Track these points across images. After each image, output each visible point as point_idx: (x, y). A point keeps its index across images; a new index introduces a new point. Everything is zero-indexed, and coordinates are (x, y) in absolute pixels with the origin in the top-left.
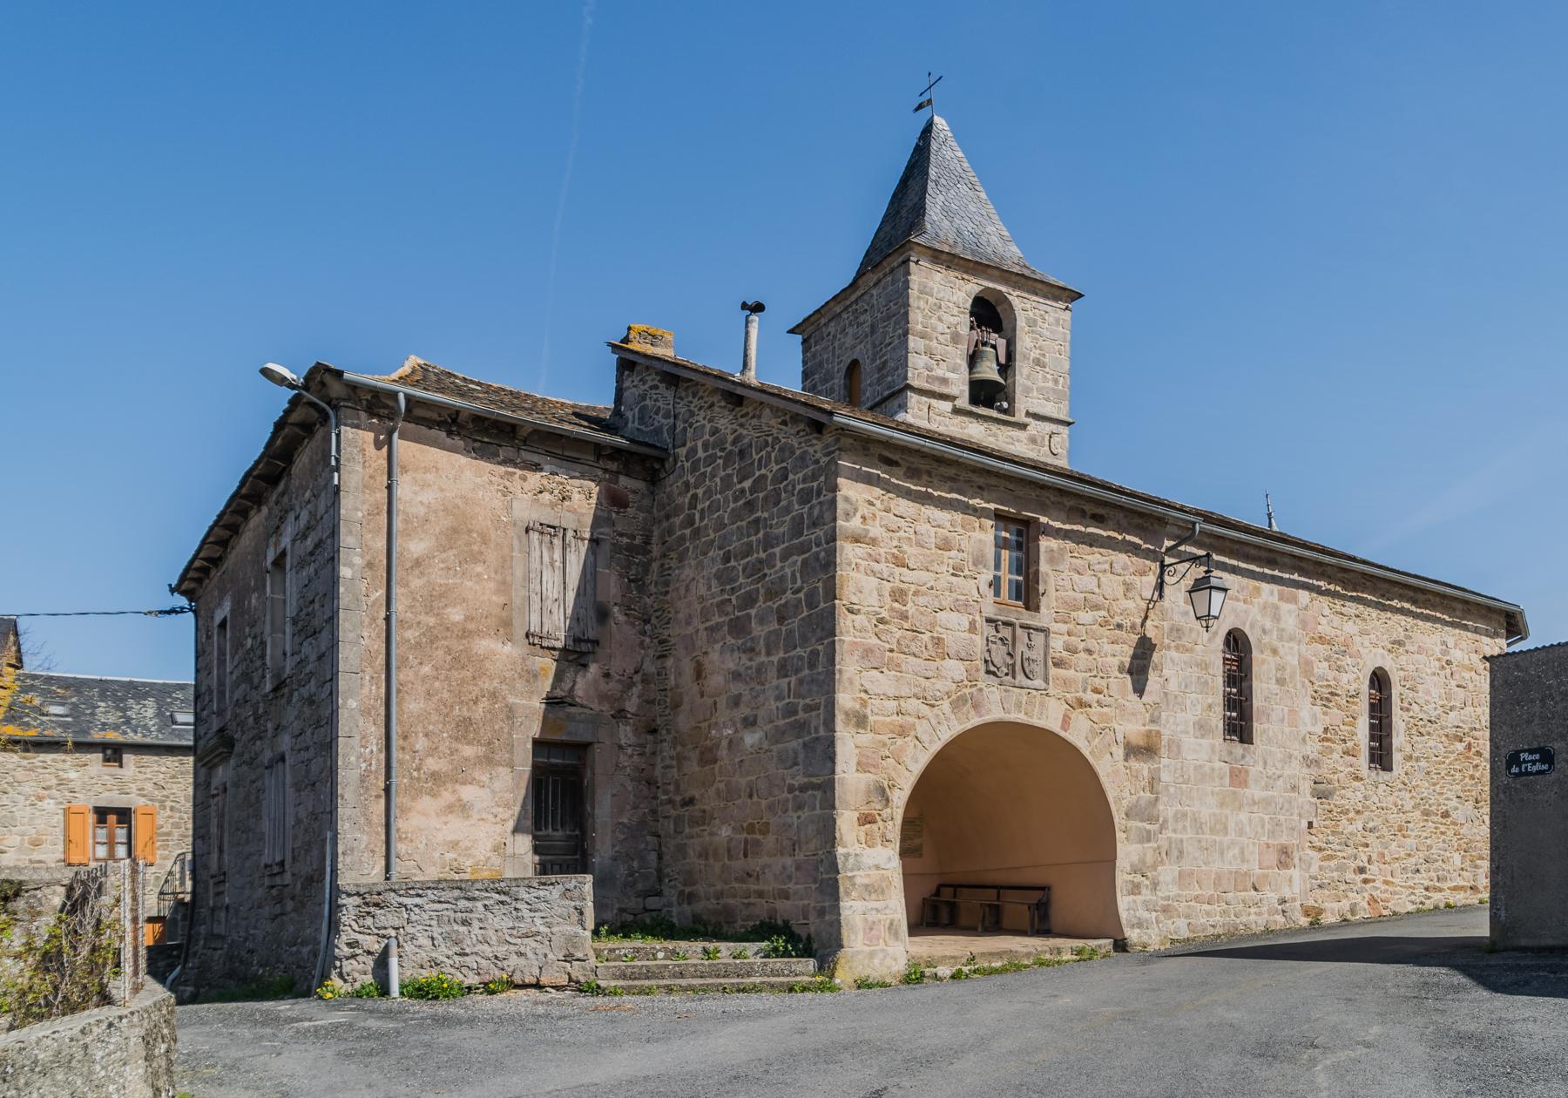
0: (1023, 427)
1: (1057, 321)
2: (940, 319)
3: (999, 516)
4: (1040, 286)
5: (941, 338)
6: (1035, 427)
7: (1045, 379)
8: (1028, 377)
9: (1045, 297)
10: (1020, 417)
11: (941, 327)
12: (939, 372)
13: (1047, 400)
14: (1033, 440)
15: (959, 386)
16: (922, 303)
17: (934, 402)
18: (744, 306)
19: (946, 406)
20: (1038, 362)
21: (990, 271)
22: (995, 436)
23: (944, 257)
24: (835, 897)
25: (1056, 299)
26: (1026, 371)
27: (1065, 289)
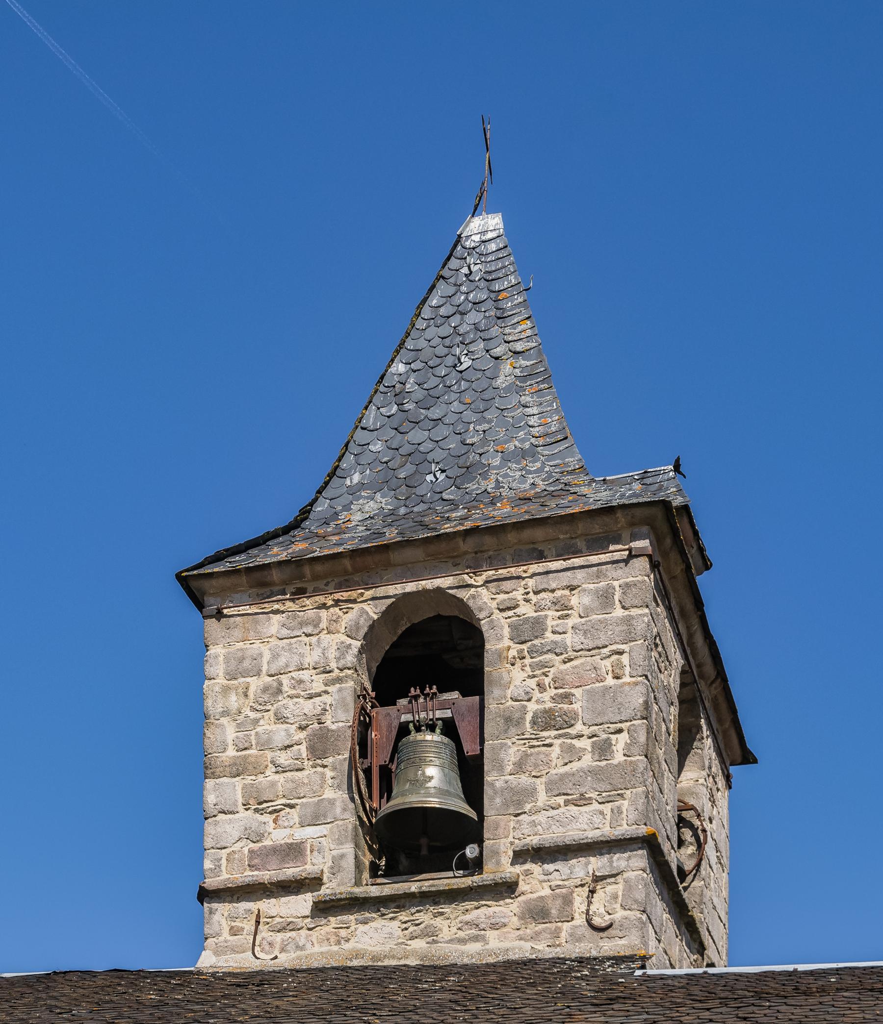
0: (506, 889)
1: (605, 598)
2: (280, 719)
3: (473, 216)
4: (539, 533)
5: (284, 758)
6: (536, 882)
7: (571, 754)
8: (520, 767)
9: (567, 551)
10: (500, 866)
11: (280, 734)
12: (278, 836)
13: (582, 801)
14: (538, 913)
15: (334, 850)
16: (234, 701)
17: (269, 906)
18: (677, 461)
19: (303, 903)
20: (547, 720)
21: (395, 556)
22: (431, 934)
23: (276, 575)
24: (371, 898)
25: (598, 544)
26: (512, 753)
27: (608, 510)
